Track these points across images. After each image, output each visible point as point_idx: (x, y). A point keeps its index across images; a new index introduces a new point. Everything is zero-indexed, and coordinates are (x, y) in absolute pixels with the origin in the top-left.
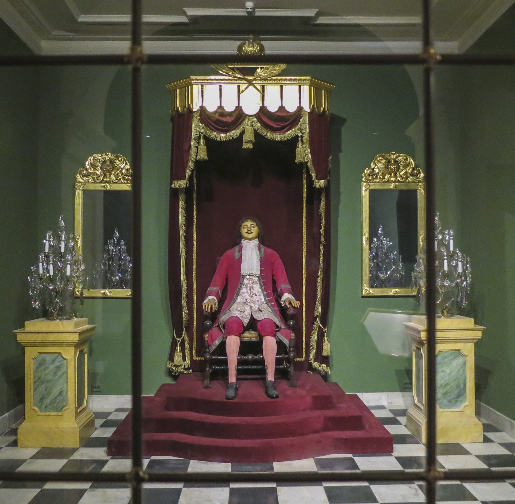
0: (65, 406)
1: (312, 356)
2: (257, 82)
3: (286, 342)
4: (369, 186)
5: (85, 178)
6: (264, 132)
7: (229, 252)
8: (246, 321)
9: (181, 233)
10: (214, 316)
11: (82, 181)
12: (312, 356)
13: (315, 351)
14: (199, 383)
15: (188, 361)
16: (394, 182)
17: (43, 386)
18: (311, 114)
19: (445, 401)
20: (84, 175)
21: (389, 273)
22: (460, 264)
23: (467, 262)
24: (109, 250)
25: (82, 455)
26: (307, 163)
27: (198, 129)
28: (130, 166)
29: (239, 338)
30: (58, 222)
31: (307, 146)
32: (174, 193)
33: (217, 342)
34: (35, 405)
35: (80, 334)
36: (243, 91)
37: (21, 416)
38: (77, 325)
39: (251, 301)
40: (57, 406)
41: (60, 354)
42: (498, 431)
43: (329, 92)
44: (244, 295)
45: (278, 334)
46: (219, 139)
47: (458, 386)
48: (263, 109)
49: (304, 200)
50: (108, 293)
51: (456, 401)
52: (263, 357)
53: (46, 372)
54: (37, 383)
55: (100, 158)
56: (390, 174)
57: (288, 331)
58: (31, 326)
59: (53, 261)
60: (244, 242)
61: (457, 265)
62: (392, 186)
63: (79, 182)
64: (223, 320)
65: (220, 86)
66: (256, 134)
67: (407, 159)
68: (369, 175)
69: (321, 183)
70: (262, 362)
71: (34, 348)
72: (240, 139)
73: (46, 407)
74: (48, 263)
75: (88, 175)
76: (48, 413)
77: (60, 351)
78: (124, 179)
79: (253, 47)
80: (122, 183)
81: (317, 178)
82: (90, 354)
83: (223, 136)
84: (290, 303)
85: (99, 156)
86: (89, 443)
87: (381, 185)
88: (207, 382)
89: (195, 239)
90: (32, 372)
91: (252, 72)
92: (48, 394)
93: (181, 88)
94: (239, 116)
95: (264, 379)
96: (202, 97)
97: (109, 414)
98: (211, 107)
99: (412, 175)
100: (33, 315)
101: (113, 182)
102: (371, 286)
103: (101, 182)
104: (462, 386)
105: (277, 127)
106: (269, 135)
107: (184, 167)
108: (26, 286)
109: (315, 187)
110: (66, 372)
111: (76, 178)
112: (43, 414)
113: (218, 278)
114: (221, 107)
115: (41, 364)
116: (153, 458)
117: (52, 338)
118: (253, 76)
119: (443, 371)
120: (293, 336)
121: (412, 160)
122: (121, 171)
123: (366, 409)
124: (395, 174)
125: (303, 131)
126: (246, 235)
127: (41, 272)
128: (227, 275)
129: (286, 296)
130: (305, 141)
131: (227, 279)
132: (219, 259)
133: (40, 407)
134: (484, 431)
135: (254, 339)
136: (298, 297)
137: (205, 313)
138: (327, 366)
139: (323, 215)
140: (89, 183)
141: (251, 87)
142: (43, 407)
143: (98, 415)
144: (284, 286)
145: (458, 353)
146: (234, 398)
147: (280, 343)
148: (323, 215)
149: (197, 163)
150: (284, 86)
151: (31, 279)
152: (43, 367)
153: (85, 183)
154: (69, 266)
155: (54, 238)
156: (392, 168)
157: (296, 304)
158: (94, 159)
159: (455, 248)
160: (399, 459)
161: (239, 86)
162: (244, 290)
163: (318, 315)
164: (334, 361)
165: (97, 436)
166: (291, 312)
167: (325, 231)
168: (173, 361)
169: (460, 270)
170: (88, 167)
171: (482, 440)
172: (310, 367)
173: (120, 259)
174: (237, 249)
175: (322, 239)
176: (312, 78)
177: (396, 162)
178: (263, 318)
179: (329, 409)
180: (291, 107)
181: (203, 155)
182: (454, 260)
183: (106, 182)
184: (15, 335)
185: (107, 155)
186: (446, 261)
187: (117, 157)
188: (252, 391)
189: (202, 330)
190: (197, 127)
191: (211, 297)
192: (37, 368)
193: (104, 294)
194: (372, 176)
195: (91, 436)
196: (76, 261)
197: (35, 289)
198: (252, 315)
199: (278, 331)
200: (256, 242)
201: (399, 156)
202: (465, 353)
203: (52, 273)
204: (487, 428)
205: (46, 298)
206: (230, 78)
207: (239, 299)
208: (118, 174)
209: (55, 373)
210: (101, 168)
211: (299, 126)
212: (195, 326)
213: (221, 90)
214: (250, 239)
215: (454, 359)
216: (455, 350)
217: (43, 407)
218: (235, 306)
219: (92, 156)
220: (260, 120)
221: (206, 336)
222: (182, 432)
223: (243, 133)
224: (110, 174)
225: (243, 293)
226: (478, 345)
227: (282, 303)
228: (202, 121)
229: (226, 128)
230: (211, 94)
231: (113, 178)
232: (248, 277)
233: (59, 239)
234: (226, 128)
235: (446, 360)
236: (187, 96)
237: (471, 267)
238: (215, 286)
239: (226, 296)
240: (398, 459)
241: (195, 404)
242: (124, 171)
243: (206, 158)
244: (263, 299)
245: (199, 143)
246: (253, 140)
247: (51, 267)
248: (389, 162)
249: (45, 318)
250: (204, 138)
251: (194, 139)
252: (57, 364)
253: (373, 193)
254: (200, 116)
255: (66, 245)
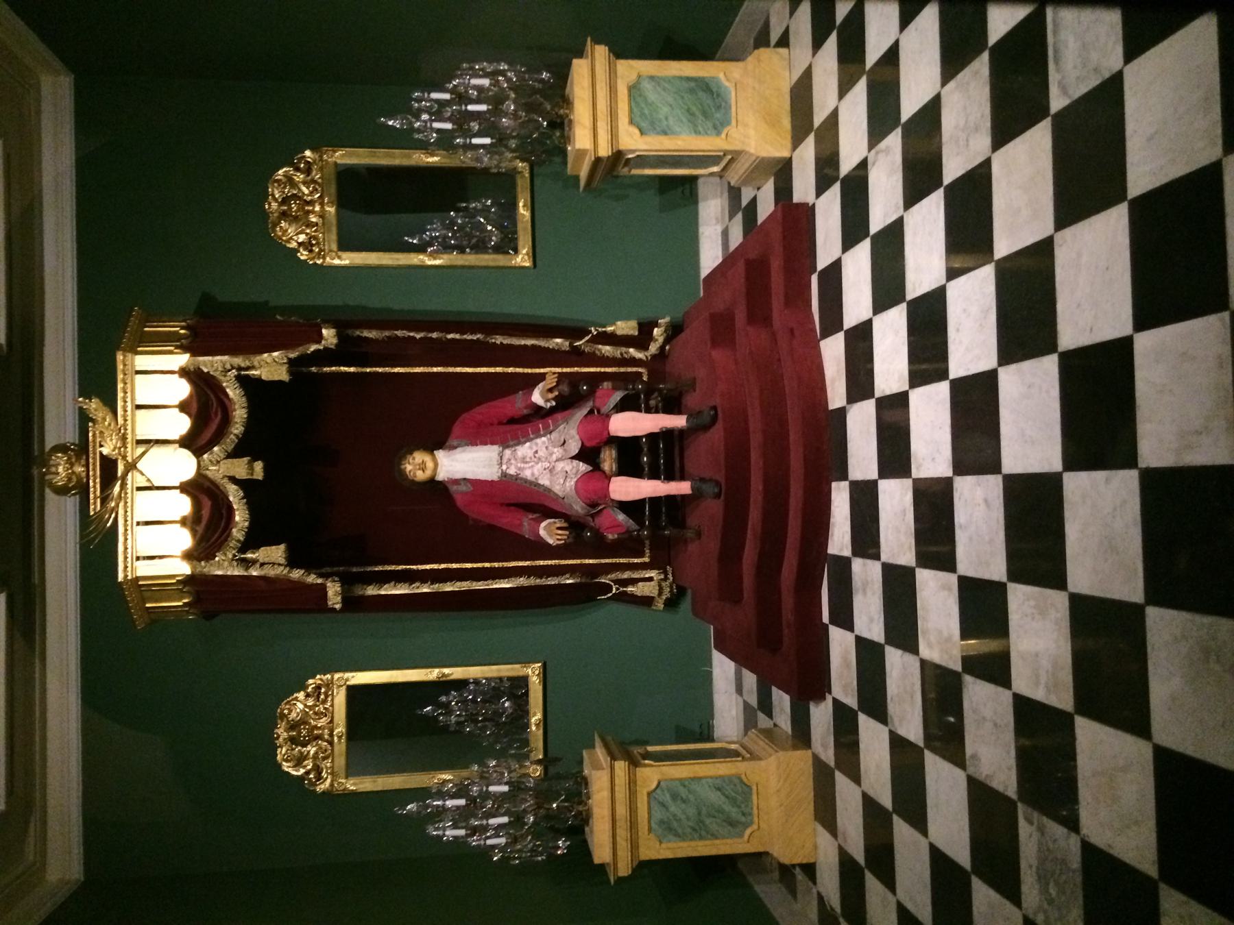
0: (741, 781)
1: (639, 355)
2: (129, 454)
3: (618, 396)
4: (331, 251)
5: (324, 774)
6: (231, 441)
7: (460, 502)
8: (583, 467)
9: (425, 590)
10: (575, 525)
11: (329, 781)
12: (639, 355)
13: (631, 350)
14: (693, 548)
15: (653, 574)
16: (322, 204)
17: (708, 821)
18: (195, 350)
19: (718, 115)
20: (319, 777)
21: (489, 228)
22: (475, 81)
23: (472, 68)
24: (458, 723)
25: (824, 746)
26: (290, 359)
27: (226, 563)
28: (299, 691)
29: (613, 479)
30: (410, 815)
31: (256, 360)
32: (352, 603)
33: (621, 517)
34: (741, 835)
35: (613, 758)
36: (149, 480)
37: (759, 859)
38: (597, 766)
39: (546, 461)
40: (739, 792)
41: (649, 794)
42: (766, 25)
43: (146, 321)
44: (536, 473)
45: (604, 410)
46: (247, 524)
47: (692, 91)
48: (187, 442)
49: (360, 370)
50: (536, 717)
51: (718, 95)
52: (646, 436)
53: (683, 817)
54: (703, 833)
55: (284, 750)
56: (308, 212)
57: (598, 393)
58: (601, 852)
59: (481, 819)
60: (441, 476)
61: (475, 87)
62: (331, 210)
63: (332, 785)
64: (582, 508)
65: (138, 524)
66: (234, 454)
67: (278, 181)
68: (311, 251)
69: (329, 335)
70: (652, 437)
71: (641, 842)
72: (246, 485)
73: (744, 814)
74: (485, 829)
75: (317, 770)
76: (755, 811)
77: (645, 793)
78: (324, 702)
79: (57, 466)
80: (332, 705)
81: (319, 342)
82: (647, 743)
83: (241, 517)
84: (551, 390)
85: (282, 752)
86: (802, 734)
87: (329, 231)
88: (689, 534)
89: (435, 566)
90: (684, 844)
91: (108, 465)
92: (720, 811)
93: (144, 601)
94: (198, 488)
95: (681, 432)
96: (161, 557)
97: (746, 705)
98: (184, 539)
99: (308, 171)
100: (581, 848)
101: (332, 721)
102: (516, 251)
103: (331, 743)
104: (693, 84)
105: (219, 416)
106: (237, 429)
107: (300, 586)
108: (528, 868)
109: (336, 345)
110: (680, 780)
111: (324, 792)
112: (756, 819)
113: (506, 520)
114: (183, 522)
115: (668, 828)
116: (826, 618)
117: (622, 810)
118: (116, 461)
119: (666, 119)
120: (607, 385)
121: (280, 172)
122: (310, 708)
123: (729, 260)
124: (311, 203)
125: (228, 367)
126: (428, 473)
127: (502, 841)
128: (502, 505)
129: (537, 397)
130: (248, 363)
131: (509, 505)
132: (474, 520)
133: (747, 825)
134: (767, 45)
135: (614, 453)
136: (532, 382)
137: (571, 540)
138: (656, 325)
139: (387, 333)
140: (332, 767)
141: (138, 465)
142: (743, 819)
143: (749, 722)
144: (516, 405)
145: (633, 89)
146: (718, 483)
147: (622, 407)
148: (387, 333)
149: (292, 563)
150: (138, 402)
151: (515, 858)
152: (675, 824)
153: (332, 774)
154: (492, 789)
155: (441, 821)
156: (295, 210)
157: (551, 381)
158: (287, 761)
159: (442, 90)
160: (821, 189)
161: (139, 489)
162: (527, 474)
163: (567, 343)
164: (647, 315)
165: (789, 723)
166: (565, 388)
167: (418, 329)
168: (653, 598)
169: (485, 82)
170: (302, 771)
171: (783, 51)
172: (662, 355)
173: (474, 701)
174: (453, 488)
175: (435, 335)
176: (118, 348)
177: (285, 201)
178: (577, 437)
179: (732, 319)
180: (182, 389)
181: (277, 553)
182: (467, 92)
183: (331, 735)
184: (620, 880)
185: (279, 737)
186: (470, 108)
187: (283, 716)
188: (707, 451)
189: (600, 546)
190: (223, 566)
191: (542, 533)
192: (677, 835)
193: (537, 725)
194: (312, 245)
195: (789, 731)
196: (482, 777)
197: (534, 851)
198: (573, 458)
199: (599, 411)
200: (440, 454)
201: (273, 195)
202: (634, 77)
203: (505, 820)
204: (762, 40)
205: (552, 826)
206: (121, 505)
207: (545, 481)
208: (316, 713)
209: (684, 801)
210: (304, 745)
211: (216, 374)
212: (591, 561)
213: (147, 523)
214: (436, 465)
215: (645, 99)
216: (630, 95)
217: (743, 819)
218: (557, 489)
219: (280, 766)
220: (207, 447)
221: (610, 537)
222: (779, 571)
223: (233, 480)
224: (316, 727)
225: (533, 474)
226: (620, 52)
227: (549, 405)
228: (209, 557)
229: (224, 512)
230: (157, 541)
231: (323, 722)
232: (504, 467)
233: (441, 813)
234: (224, 512)
235: (646, 112)
236: (159, 588)
237: (477, 62)
238: (521, 525)
239: (537, 503)
240: (819, 192)
241: (730, 554)
242: (310, 702)
243: (282, 547)
244: (544, 439)
245: (254, 562)
246: (246, 459)
247: (494, 821)
248: (284, 215)
249: (587, 829)
250: (244, 553)
251: (247, 569)
252: (667, 798)
253: (346, 245)
254: (200, 561)
255: (453, 797)
